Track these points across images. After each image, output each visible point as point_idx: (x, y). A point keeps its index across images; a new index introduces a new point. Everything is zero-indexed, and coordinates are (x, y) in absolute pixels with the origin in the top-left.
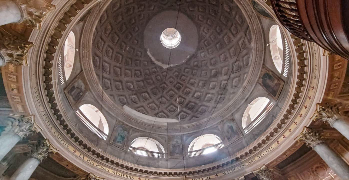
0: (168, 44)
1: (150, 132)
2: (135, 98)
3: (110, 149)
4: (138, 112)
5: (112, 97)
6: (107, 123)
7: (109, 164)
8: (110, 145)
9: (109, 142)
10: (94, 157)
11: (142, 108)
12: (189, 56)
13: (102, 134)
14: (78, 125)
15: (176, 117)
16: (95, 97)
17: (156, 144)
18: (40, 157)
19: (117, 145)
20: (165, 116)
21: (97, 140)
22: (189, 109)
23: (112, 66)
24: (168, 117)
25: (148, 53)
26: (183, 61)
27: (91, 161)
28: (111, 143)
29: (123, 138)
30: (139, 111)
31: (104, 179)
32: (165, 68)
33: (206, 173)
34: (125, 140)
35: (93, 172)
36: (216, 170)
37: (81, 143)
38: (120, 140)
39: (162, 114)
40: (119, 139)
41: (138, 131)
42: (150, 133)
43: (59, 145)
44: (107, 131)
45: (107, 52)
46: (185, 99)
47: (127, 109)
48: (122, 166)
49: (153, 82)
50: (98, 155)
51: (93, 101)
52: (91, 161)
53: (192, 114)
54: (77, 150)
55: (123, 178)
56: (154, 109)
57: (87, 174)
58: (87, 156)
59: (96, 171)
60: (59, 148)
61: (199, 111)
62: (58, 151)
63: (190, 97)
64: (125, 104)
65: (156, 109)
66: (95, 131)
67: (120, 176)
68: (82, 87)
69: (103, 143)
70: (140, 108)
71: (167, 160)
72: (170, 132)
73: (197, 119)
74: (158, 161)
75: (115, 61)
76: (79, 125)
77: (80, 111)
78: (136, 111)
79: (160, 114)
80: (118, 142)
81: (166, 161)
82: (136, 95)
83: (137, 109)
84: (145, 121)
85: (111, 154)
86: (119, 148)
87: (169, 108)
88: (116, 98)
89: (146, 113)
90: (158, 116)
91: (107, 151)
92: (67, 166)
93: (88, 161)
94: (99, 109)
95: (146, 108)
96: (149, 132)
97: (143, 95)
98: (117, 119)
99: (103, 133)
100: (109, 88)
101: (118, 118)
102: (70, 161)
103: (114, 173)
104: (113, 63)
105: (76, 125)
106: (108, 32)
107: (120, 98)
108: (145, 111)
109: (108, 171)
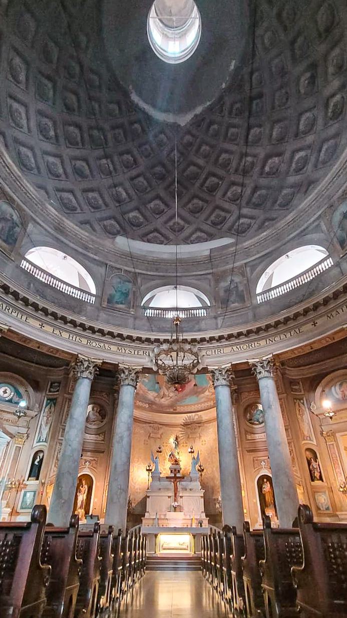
0: (159, 45)
1: (175, 274)
2: (136, 217)
3: (104, 315)
4: (149, 244)
5: (88, 226)
6: (89, 275)
7: (107, 338)
8: (103, 310)
9: (101, 305)
10: (78, 330)
11: (156, 234)
12: (234, 61)
13: (85, 294)
14: (32, 285)
15: (229, 232)
16: (48, 232)
17: (196, 296)
18: (86, 374)
19: (116, 308)
20: (205, 236)
21: (76, 305)
22: (257, 206)
23: (67, 161)
24: (211, 237)
25: (135, 98)
26: (224, 86)
27: (74, 337)
28: (104, 306)
29: (126, 295)
30: (149, 241)
31: (103, 360)
32: (183, 124)
33: (291, 324)
34: (130, 296)
35: (82, 353)
36: (312, 315)
37: (45, 311)
38: (120, 300)
39: (199, 234)
40: (117, 297)
41: (153, 278)
42: (177, 276)
43: (9, 319)
44: (93, 290)
45: (274, 173)
46: (243, 185)
47: (122, 242)
48: (130, 338)
49: (135, 161)
50: (82, 326)
51: (51, 240)
52: (74, 337)
53: (262, 217)
54: (46, 323)
55: (138, 356)
56: (182, 229)
57: (75, 357)
58: (66, 331)
59: (88, 350)
60: (10, 322)
61: (206, 187)
62: (10, 327)
63: (255, 177)
64: (118, 233)
65: (185, 228)
66: (78, 294)
67: (133, 353)
68: (13, 216)
69: (89, 308)
70: (151, 235)
71: (216, 318)
72: (217, 266)
73: (274, 221)
74: (198, 322)
75: (93, 147)
76: (34, 284)
77: (28, 261)
78: (144, 241)
79: (195, 236)
80: (117, 303)
81: (214, 319)
82: (137, 211)
83: (145, 239)
84: (165, 256)
85: (108, 323)
86: (120, 313)
87: (212, 218)
88: (97, 227)
89: (165, 242)
90: (191, 241)
91: (100, 318)
92: (39, 347)
93: (71, 338)
94: (66, 254)
95: (163, 231)
96: (172, 275)
97: (152, 205)
98: (107, 264)
99: (90, 294)
100: (76, 210)
101: (107, 262)
102: (39, 340)
103: (121, 351)
104: (68, 152)
105: (29, 288)
106: (22, 77)
107: (104, 225)
108: (162, 239)
109: (109, 348)
